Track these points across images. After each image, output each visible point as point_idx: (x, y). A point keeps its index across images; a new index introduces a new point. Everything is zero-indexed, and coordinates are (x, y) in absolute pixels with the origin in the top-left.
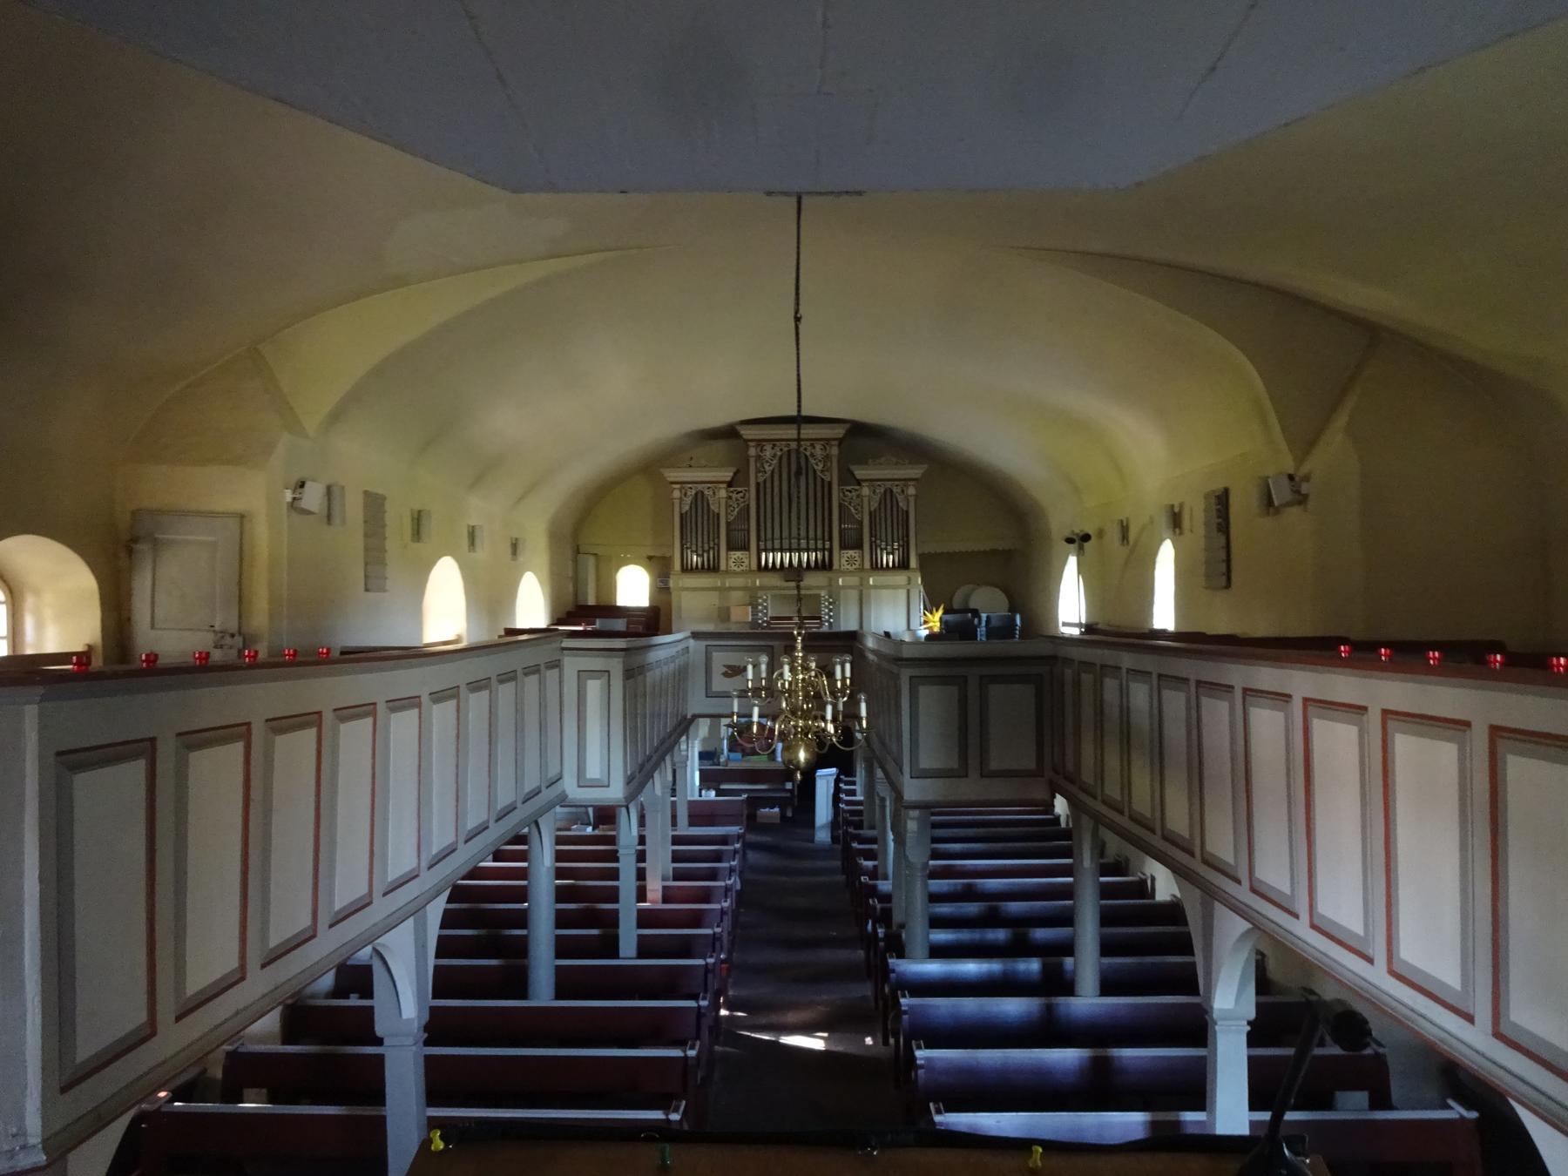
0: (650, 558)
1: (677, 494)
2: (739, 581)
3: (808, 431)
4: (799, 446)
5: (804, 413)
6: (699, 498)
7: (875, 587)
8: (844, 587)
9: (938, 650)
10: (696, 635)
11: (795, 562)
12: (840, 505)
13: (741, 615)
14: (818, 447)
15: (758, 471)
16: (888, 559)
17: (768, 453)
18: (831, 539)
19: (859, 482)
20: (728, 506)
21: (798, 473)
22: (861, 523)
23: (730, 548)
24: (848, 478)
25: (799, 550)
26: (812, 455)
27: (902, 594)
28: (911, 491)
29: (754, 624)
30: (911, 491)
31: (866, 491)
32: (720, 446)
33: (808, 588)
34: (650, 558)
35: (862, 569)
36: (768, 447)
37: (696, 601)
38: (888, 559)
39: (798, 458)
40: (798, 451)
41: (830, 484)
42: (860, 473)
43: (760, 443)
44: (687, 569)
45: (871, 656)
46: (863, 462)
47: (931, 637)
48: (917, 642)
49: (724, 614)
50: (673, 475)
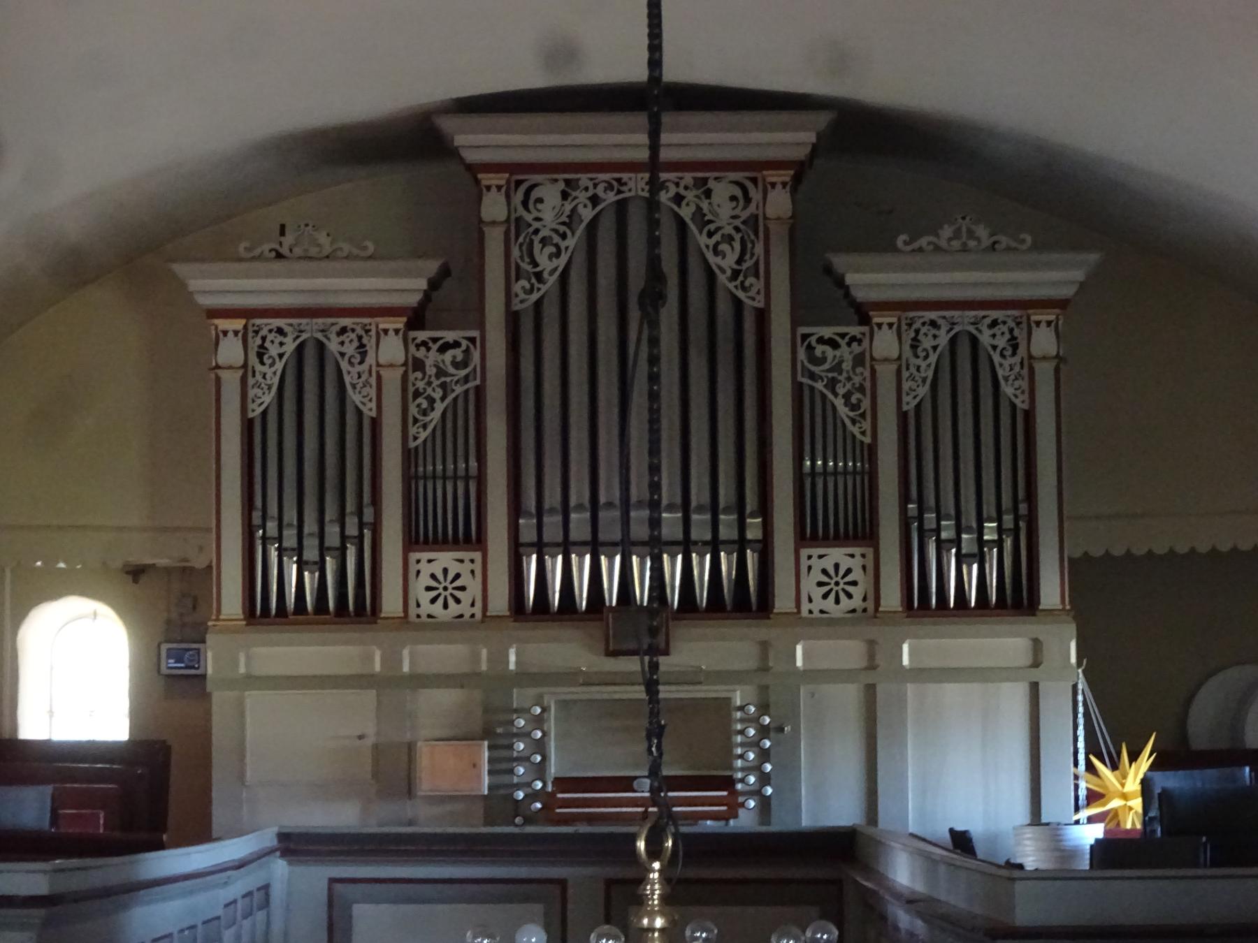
0: (136, 573)
1: (231, 351)
2: (446, 655)
3: (688, 138)
4: (655, 186)
5: (673, 72)
6: (312, 363)
7: (920, 674)
8: (812, 675)
9: (1139, 898)
10: (294, 845)
11: (642, 592)
12: (798, 389)
13: (454, 774)
14: (722, 191)
15: (512, 273)
16: (965, 577)
17: (550, 205)
18: (765, 509)
19: (862, 314)
20: (408, 394)
21: (653, 297)
22: (872, 450)
23: (414, 540)
24: (823, 296)
25: (655, 547)
26: (701, 219)
27: (1014, 698)
28: (1044, 342)
29: (499, 804)
30: (1044, 342)
31: (885, 343)
32: (378, 194)
33: (693, 677)
34: (136, 573)
35: (872, 612)
36: (550, 194)
37: (295, 720)
38: (965, 577)
39: (653, 224)
40: (652, 204)
41: (762, 317)
42: (868, 278)
43: (520, 176)
44: (263, 612)
45: (904, 919)
46: (877, 241)
47: (1112, 852)
48: (1061, 873)
49: (393, 771)
50: (215, 285)
